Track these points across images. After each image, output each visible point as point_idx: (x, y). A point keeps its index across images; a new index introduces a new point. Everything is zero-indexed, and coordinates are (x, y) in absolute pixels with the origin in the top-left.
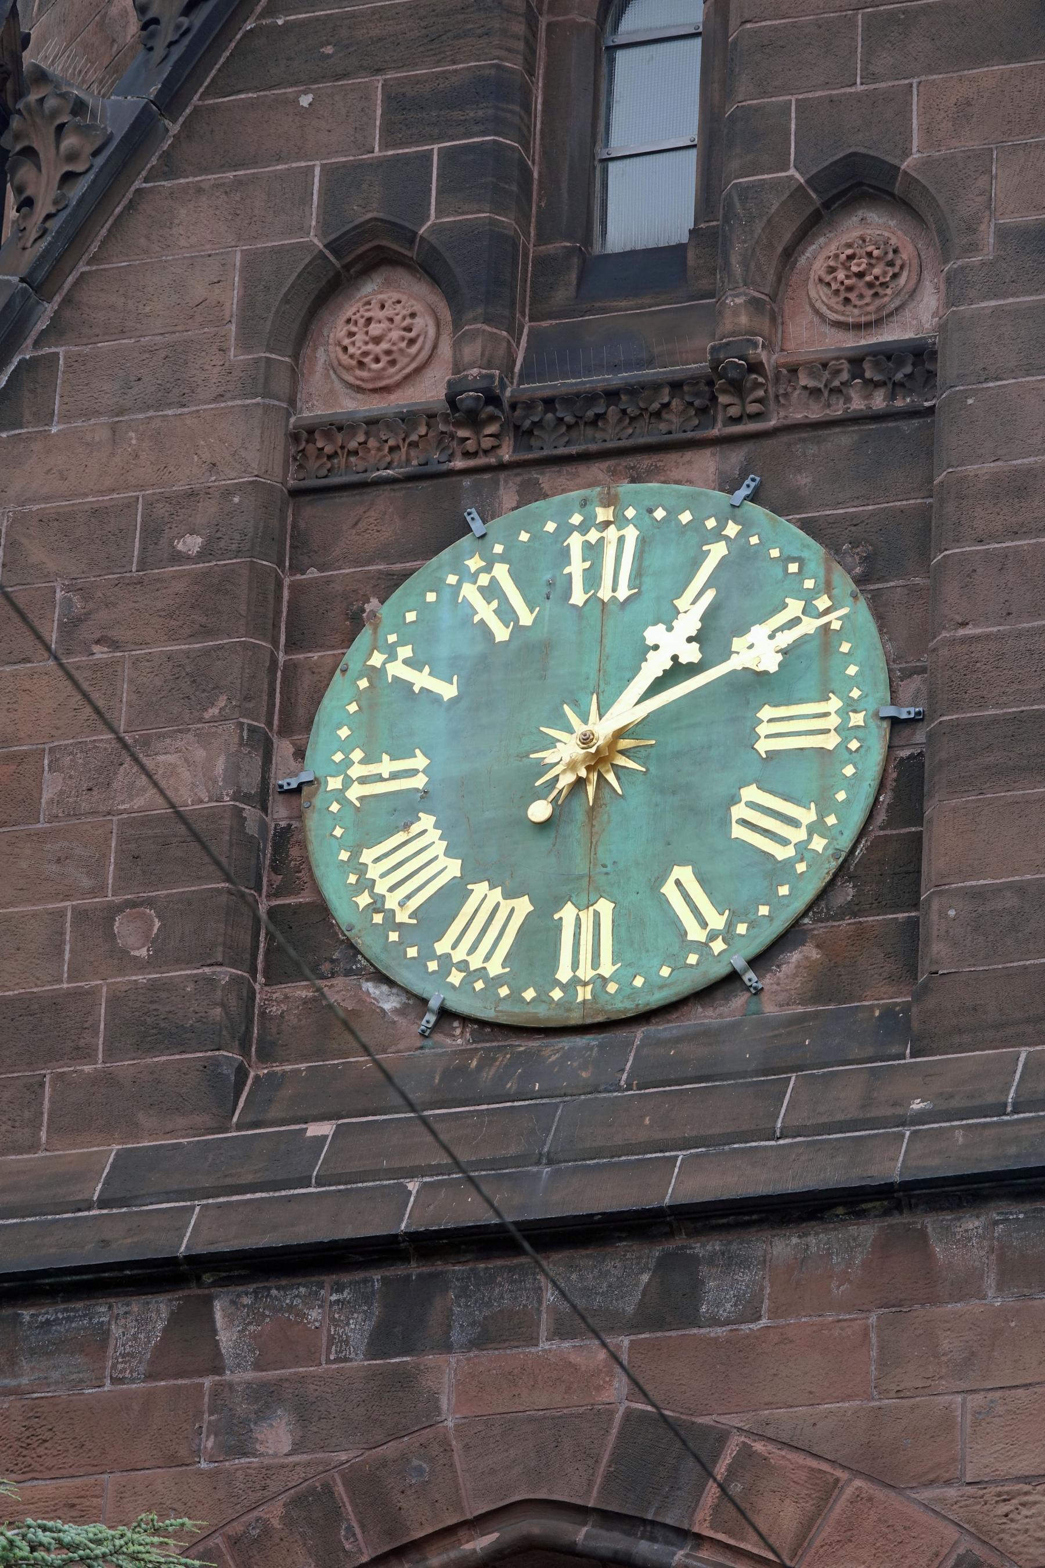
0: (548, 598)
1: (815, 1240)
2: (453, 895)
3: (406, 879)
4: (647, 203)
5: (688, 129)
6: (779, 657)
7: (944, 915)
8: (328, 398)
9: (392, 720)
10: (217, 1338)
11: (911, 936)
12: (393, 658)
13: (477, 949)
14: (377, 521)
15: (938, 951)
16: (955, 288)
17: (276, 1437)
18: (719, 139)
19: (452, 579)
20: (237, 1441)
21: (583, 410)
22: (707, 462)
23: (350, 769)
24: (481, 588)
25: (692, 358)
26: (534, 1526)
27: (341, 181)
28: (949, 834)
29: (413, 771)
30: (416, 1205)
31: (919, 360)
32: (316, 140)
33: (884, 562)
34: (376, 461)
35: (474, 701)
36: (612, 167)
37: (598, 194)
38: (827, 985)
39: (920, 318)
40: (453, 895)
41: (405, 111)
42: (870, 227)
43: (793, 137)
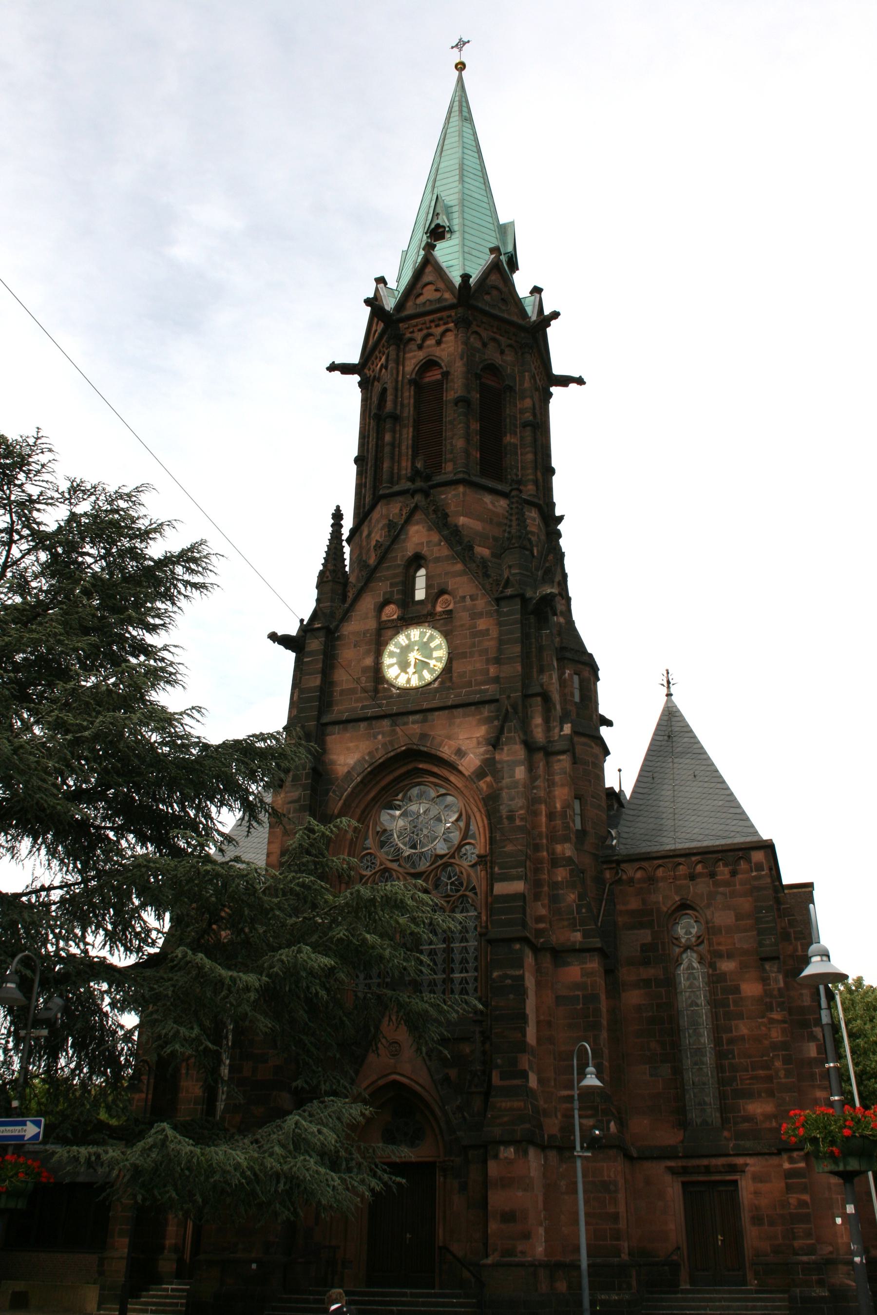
0: (38, 428)
1: (441, 713)
2: (399, 675)
3: (392, 672)
4: (420, 594)
5: (424, 586)
6: (558, 513)
7: (455, 675)
8: (384, 618)
9: (392, 655)
10: (133, 1012)
11: (451, 677)
12: (391, 647)
13: (401, 681)
14: (390, 632)
15: (454, 679)
16: (455, 603)
17: (380, 737)
18: (428, 587)
19: (18, 470)
20: (375, 738)
21: (412, 618)
22: (426, 624)
23: (387, 661)
24: (402, 639)
25: (425, 612)
26: (410, 746)
27: (385, 593)
28: (455, 665)
29: (394, 660)
30: (395, 709)
31: (451, 611)
32: (382, 588)
33: (446, 635)
34: (389, 625)
35: (401, 652)
36: (354, 358)
37: (487, 832)
38: (442, 683)
39: (450, 607)
40: (399, 675)
41: (392, 585)
42: (446, 596)
43: (380, 1290)
